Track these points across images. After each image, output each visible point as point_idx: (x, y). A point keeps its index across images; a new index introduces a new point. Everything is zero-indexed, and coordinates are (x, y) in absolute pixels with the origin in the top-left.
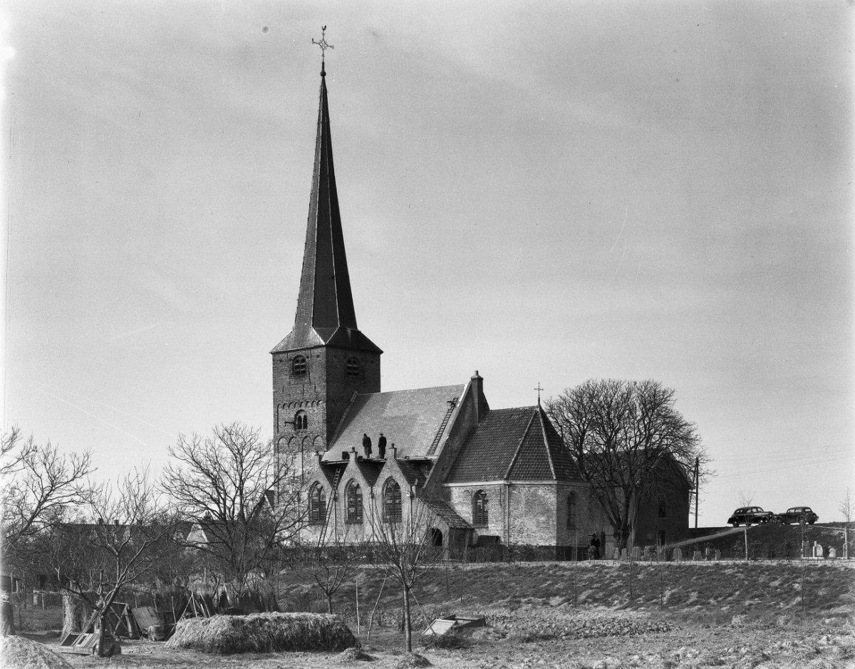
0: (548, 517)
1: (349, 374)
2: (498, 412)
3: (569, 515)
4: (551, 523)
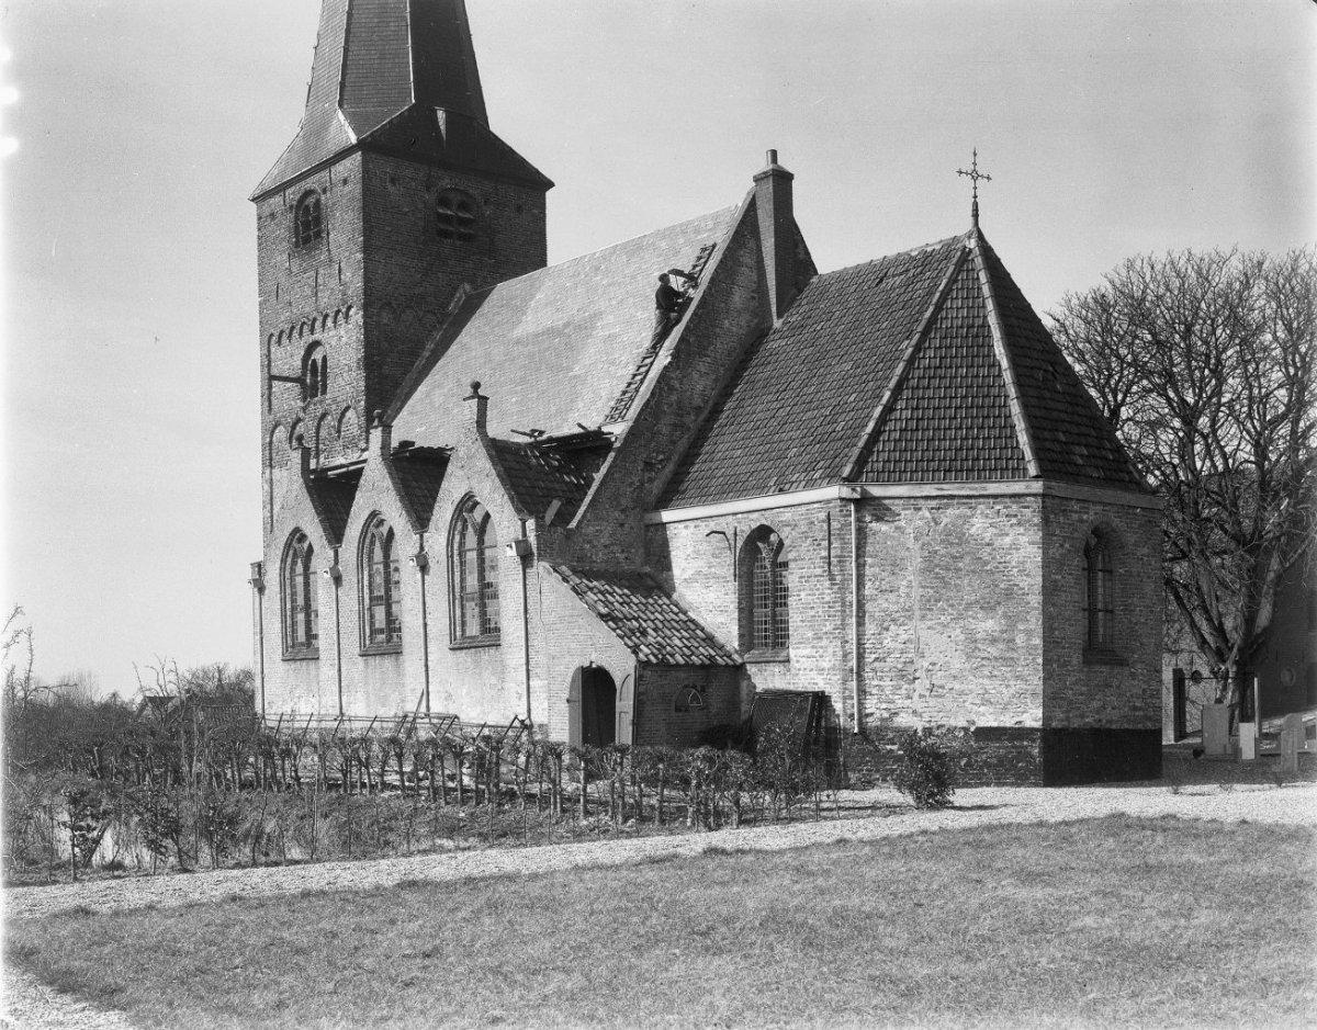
0: (1012, 621)
1: (445, 234)
2: (840, 277)
3: (1091, 611)
4: (1020, 640)
